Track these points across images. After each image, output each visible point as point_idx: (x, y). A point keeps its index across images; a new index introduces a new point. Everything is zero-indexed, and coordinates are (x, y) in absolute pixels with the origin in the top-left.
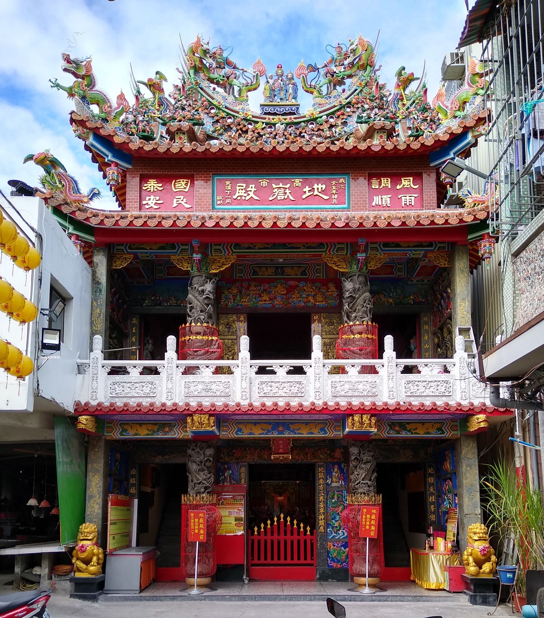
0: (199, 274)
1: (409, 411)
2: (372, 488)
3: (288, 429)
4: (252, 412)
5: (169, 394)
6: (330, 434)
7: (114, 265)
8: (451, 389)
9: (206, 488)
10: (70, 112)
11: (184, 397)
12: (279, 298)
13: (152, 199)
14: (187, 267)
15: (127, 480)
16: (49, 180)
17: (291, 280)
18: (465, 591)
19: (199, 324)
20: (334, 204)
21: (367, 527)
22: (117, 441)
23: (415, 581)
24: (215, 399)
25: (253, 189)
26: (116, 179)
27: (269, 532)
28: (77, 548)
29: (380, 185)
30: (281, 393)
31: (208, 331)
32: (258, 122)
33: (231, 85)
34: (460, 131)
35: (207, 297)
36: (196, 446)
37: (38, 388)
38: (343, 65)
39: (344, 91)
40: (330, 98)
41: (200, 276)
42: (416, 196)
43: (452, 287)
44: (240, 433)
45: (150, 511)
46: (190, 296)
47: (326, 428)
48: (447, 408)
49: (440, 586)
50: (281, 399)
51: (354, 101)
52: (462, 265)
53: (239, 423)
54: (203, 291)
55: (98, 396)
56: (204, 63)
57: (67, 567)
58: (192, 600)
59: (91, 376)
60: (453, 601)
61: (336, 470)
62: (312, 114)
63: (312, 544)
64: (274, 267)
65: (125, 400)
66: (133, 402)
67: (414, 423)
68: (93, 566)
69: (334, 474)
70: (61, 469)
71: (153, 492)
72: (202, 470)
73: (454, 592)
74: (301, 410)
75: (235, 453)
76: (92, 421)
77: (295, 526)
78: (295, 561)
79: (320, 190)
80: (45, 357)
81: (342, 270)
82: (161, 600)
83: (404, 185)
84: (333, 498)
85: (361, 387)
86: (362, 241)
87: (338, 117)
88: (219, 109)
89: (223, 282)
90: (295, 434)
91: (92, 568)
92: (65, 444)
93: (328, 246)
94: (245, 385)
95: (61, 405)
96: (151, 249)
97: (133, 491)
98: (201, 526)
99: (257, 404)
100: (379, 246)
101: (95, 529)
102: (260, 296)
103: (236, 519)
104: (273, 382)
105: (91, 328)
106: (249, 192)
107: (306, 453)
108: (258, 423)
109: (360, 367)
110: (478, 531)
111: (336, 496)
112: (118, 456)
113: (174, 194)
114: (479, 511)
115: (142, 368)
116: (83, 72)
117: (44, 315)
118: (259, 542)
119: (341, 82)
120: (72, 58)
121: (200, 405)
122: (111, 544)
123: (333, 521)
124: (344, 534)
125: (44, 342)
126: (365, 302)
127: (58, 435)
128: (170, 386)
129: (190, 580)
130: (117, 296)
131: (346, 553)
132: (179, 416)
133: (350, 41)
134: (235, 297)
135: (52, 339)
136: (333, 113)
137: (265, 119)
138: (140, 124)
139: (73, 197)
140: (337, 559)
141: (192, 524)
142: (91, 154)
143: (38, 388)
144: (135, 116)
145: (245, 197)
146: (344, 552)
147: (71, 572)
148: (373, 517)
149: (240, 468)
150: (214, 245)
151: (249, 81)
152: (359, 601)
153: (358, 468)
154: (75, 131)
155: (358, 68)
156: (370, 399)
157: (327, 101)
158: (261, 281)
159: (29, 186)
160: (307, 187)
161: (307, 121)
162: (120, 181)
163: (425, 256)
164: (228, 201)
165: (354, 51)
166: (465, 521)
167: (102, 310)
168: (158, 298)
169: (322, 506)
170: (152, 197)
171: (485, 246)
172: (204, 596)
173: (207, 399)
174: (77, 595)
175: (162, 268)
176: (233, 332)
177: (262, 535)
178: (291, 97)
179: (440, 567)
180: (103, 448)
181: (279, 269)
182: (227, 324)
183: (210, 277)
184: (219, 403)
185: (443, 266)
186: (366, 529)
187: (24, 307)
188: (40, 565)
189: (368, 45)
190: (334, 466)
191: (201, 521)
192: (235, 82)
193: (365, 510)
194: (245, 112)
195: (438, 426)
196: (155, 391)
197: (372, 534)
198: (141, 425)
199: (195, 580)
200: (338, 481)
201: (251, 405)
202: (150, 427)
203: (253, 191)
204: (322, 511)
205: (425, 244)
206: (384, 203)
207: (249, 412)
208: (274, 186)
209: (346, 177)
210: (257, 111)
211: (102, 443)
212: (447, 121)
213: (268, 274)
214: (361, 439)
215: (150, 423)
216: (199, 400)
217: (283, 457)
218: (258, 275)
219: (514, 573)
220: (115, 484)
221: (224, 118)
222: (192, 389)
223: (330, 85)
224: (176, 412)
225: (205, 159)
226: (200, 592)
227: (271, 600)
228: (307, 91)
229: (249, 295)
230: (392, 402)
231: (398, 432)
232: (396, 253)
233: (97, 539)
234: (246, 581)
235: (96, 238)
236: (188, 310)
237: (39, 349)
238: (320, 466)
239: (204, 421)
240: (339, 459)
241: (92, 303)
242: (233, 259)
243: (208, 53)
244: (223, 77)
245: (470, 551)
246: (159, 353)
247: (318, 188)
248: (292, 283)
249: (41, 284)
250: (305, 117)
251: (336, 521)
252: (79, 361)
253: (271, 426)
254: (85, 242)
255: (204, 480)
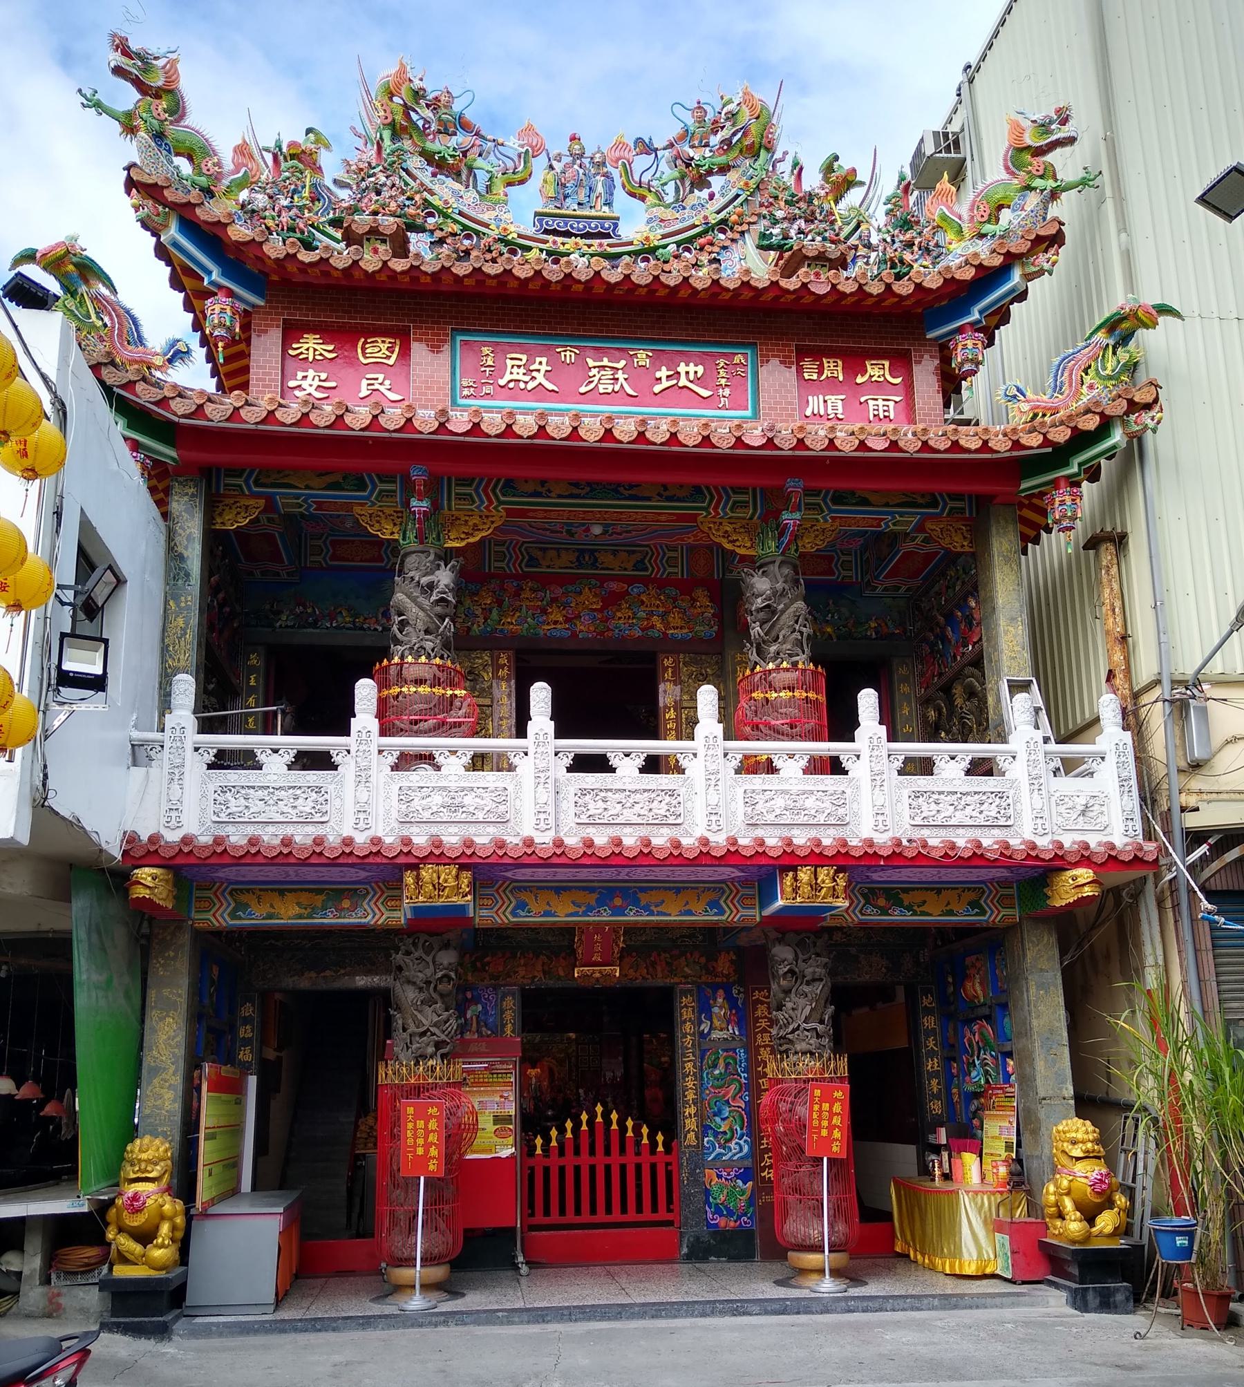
0: (421, 547)
1: (922, 859)
2: (825, 1041)
3: (636, 902)
4: (562, 860)
5: (362, 816)
6: (732, 914)
7: (219, 520)
8: (1011, 811)
9: (438, 1045)
10: (126, 164)
11: (396, 825)
12: (586, 619)
13: (310, 378)
14: (392, 533)
15: (233, 1029)
16: (73, 308)
17: (613, 580)
18: (1051, 1277)
19: (423, 659)
20: (724, 408)
21: (824, 1133)
22: (217, 933)
23: (908, 1256)
24: (472, 829)
25: (544, 368)
26: (228, 323)
27: (569, 1150)
28: (119, 1202)
29: (820, 373)
30: (629, 815)
31: (443, 676)
32: (529, 249)
33: (471, 169)
34: (997, 261)
35: (442, 600)
36: (414, 944)
37: (44, 785)
38: (707, 145)
39: (712, 196)
40: (684, 208)
41: (423, 552)
42: (898, 399)
43: (982, 593)
44: (522, 914)
45: (273, 1103)
46: (399, 596)
47: (722, 902)
48: (1008, 853)
49: (986, 1267)
50: (628, 830)
51: (734, 218)
52: (1006, 546)
53: (519, 888)
54: (431, 586)
55: (184, 819)
56: (416, 122)
57: (91, 1252)
58: (412, 1326)
59: (166, 769)
60: (1032, 1305)
61: (720, 1000)
62: (647, 239)
63: (669, 1175)
64: (578, 550)
65: (251, 830)
66: (271, 837)
67: (918, 889)
68: (162, 1246)
69: (716, 1010)
70: (81, 1000)
71: (279, 1059)
72: (430, 1002)
73: (1024, 1283)
74: (676, 857)
75: (489, 963)
76: (167, 881)
77: (630, 1133)
78: (632, 1216)
79: (692, 377)
80: (66, 707)
81: (742, 551)
82: (334, 1330)
83: (871, 376)
84: (715, 1066)
85: (810, 803)
86: (794, 485)
87: (702, 249)
88: (446, 216)
89: (474, 573)
90: (652, 914)
91: (158, 1254)
92: (95, 937)
93: (712, 497)
94: (545, 796)
95: (94, 836)
96: (307, 487)
97: (245, 1055)
98: (433, 1138)
99: (572, 841)
100: (824, 500)
101: (166, 1151)
102: (544, 611)
103: (497, 1119)
104: (610, 790)
105: (163, 661)
106: (534, 374)
107: (653, 964)
108: (565, 889)
109: (806, 758)
110: (1080, 1136)
111: (721, 1061)
112: (215, 971)
113: (362, 368)
114: (1069, 1090)
115: (293, 753)
116: (159, 82)
117: (63, 603)
118: (547, 1170)
119: (701, 182)
120: (134, 46)
121: (437, 843)
122: (205, 1189)
123: (718, 1119)
124: (741, 1150)
125: (64, 667)
126: (796, 622)
127: (80, 916)
128: (363, 796)
129: (403, 1274)
130: (221, 596)
131: (748, 1193)
132: (385, 870)
133: (722, 98)
134: (487, 612)
135: (83, 662)
136: (690, 240)
137: (546, 242)
138: (284, 214)
139: (131, 352)
140: (727, 1209)
141: (409, 1134)
142: (169, 269)
143: (44, 785)
144: (271, 197)
145: (526, 383)
146: (743, 1192)
147: (102, 1263)
148: (837, 1108)
149: (503, 999)
150: (457, 485)
151: (510, 164)
152: (817, 1313)
153: (793, 995)
154: (136, 208)
155: (741, 151)
156: (832, 832)
157: (677, 215)
158: (545, 581)
159: (37, 284)
160: (664, 368)
161: (636, 253)
162: (237, 330)
163: (920, 528)
164: (486, 390)
165: (732, 116)
166: (1042, 1114)
167: (189, 619)
168: (309, 611)
169: (690, 1084)
170: (311, 373)
171: (1062, 503)
172: (442, 1314)
173: (453, 829)
174: (118, 1325)
175: (320, 543)
176: (483, 690)
177: (555, 1155)
178: (600, 202)
179: (985, 1222)
180: (187, 948)
181: (587, 555)
182: (470, 673)
183: (446, 556)
184: (483, 838)
185: (959, 549)
186: (820, 1137)
187: (24, 560)
188: (19, 1247)
189: (763, 108)
190: (715, 992)
191: (433, 1125)
192: (480, 162)
193: (818, 1093)
194: (503, 225)
195: (971, 896)
196: (327, 807)
197: (835, 1149)
198: (282, 893)
199: (417, 1272)
200: (724, 1026)
201: (559, 843)
202: (304, 898)
203: (543, 372)
204: (691, 1096)
205: (920, 501)
206: (830, 411)
207: (555, 860)
208: (591, 363)
209: (749, 352)
210: (528, 226)
211: (185, 939)
212: (963, 244)
213: (561, 564)
214: (803, 927)
215: (306, 890)
216: (434, 830)
217: (600, 972)
218: (538, 565)
219: (1191, 1235)
220: (210, 1041)
221: (455, 235)
222: (417, 804)
223: (683, 184)
224: (378, 860)
225: (437, 294)
226: (429, 1305)
227: (609, 1319)
228: (632, 195)
229: (519, 609)
230: (882, 839)
231: (884, 911)
232: (860, 519)
233: (171, 1176)
234: (524, 1269)
235: (183, 453)
236: (395, 628)
237: (49, 685)
238: (685, 993)
239: (446, 881)
240: (727, 976)
241: (166, 602)
242: (499, 516)
243: (424, 97)
244: (454, 149)
245: (1065, 1183)
246: (337, 719)
247: (687, 373)
248: (613, 586)
249: (59, 524)
250: (631, 243)
251: (723, 1119)
252: (136, 735)
253: (595, 896)
254: (155, 461)
255: (435, 1025)
